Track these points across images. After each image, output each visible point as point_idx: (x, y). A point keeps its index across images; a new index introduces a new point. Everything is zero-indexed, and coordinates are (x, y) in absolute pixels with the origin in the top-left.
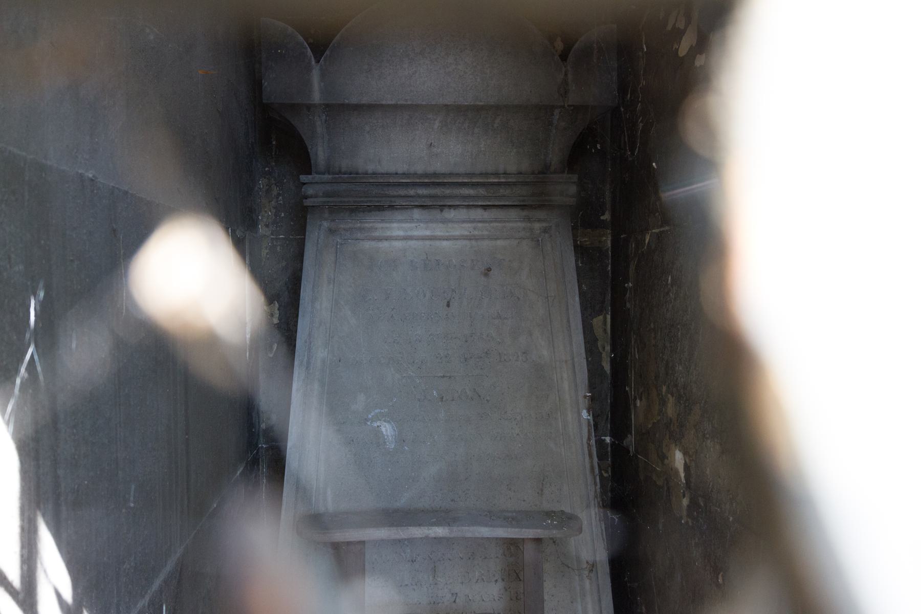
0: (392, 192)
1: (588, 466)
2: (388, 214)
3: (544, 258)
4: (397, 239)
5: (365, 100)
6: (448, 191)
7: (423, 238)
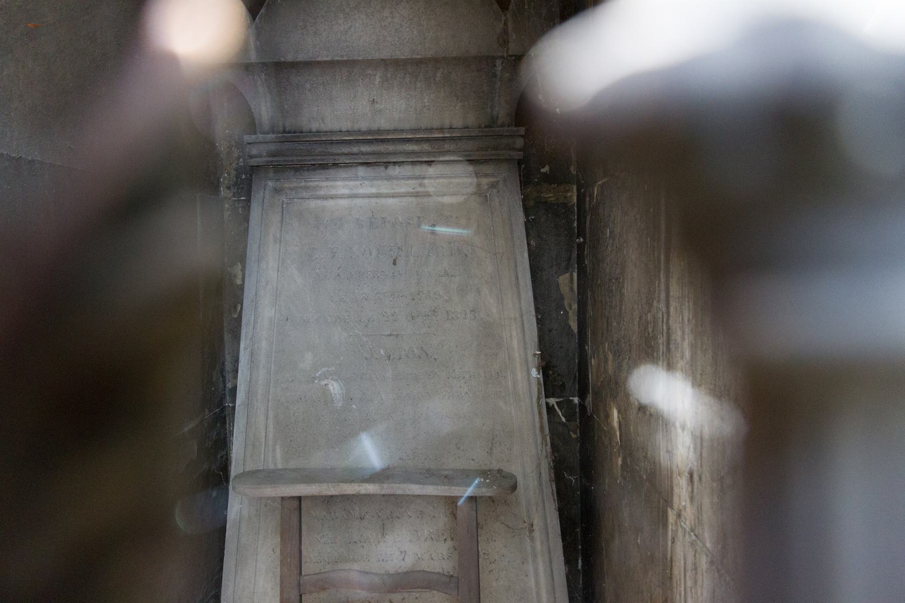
0: (336, 149)
1: (538, 425)
2: (332, 172)
3: (492, 213)
4: (342, 197)
5: (301, 57)
6: (391, 148)
7: (370, 196)
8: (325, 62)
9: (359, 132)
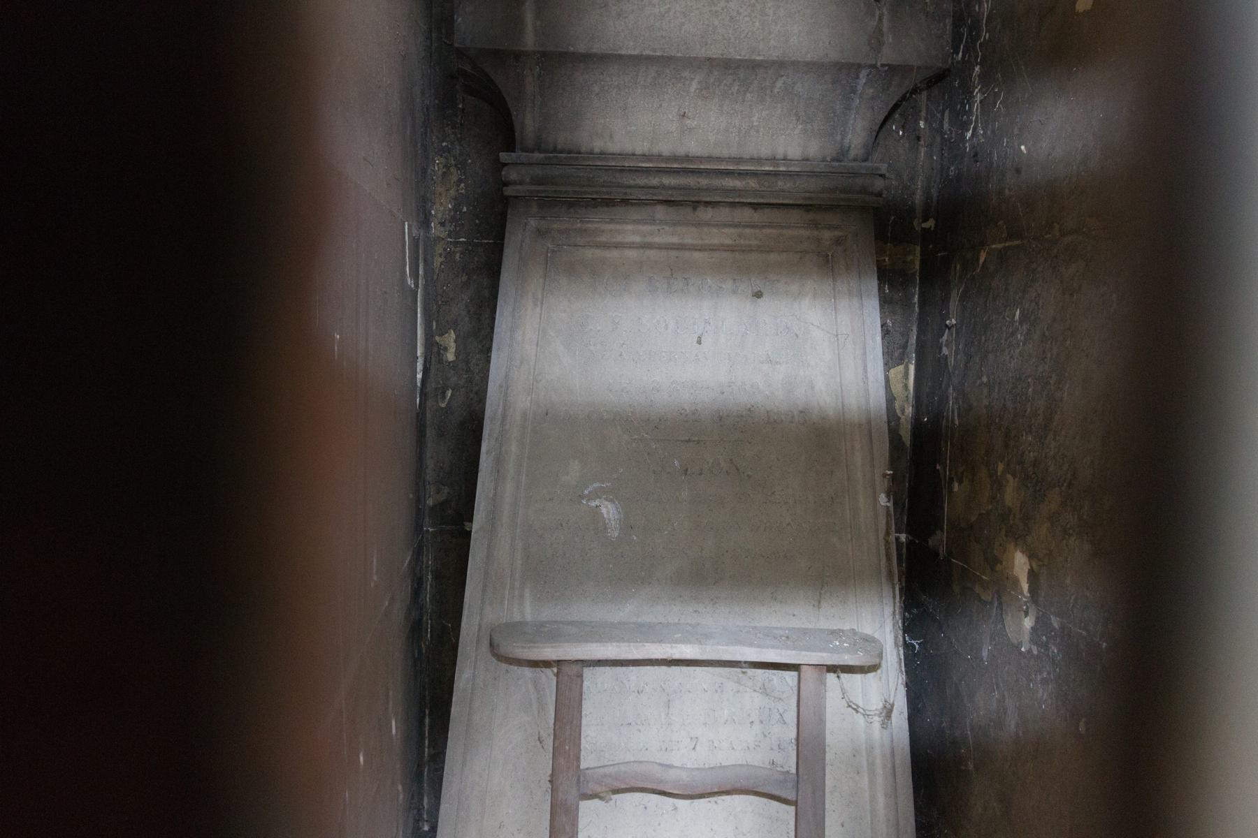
4: (631, 246)
6: (704, 182)
8: (630, 57)
9: (660, 157)
